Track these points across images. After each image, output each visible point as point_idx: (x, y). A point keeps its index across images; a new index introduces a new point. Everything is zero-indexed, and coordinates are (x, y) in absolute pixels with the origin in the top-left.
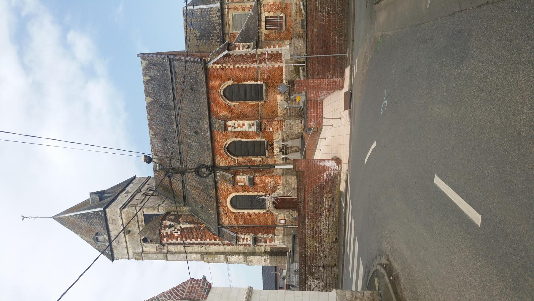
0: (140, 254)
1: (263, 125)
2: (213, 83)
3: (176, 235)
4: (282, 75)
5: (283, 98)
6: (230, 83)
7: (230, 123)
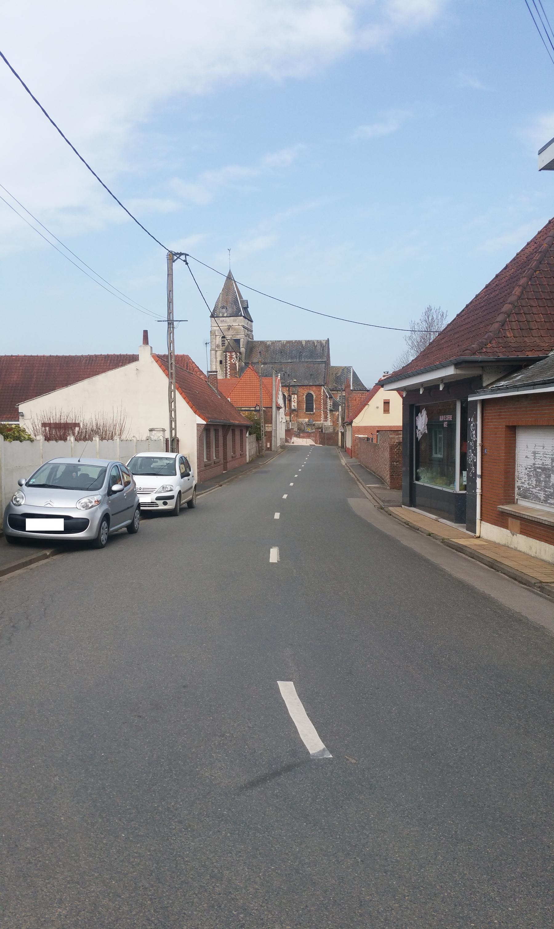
0: (215, 334)
1: (295, 412)
2: (314, 388)
3: (232, 361)
4: (317, 421)
5: (307, 421)
6: (314, 397)
7: (296, 396)
